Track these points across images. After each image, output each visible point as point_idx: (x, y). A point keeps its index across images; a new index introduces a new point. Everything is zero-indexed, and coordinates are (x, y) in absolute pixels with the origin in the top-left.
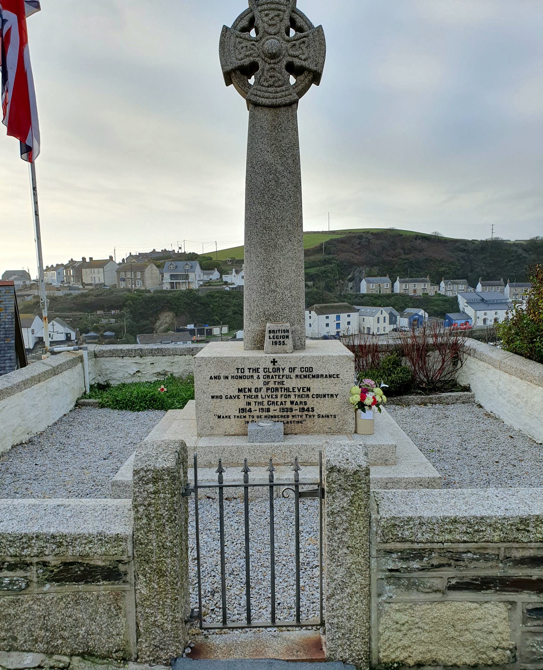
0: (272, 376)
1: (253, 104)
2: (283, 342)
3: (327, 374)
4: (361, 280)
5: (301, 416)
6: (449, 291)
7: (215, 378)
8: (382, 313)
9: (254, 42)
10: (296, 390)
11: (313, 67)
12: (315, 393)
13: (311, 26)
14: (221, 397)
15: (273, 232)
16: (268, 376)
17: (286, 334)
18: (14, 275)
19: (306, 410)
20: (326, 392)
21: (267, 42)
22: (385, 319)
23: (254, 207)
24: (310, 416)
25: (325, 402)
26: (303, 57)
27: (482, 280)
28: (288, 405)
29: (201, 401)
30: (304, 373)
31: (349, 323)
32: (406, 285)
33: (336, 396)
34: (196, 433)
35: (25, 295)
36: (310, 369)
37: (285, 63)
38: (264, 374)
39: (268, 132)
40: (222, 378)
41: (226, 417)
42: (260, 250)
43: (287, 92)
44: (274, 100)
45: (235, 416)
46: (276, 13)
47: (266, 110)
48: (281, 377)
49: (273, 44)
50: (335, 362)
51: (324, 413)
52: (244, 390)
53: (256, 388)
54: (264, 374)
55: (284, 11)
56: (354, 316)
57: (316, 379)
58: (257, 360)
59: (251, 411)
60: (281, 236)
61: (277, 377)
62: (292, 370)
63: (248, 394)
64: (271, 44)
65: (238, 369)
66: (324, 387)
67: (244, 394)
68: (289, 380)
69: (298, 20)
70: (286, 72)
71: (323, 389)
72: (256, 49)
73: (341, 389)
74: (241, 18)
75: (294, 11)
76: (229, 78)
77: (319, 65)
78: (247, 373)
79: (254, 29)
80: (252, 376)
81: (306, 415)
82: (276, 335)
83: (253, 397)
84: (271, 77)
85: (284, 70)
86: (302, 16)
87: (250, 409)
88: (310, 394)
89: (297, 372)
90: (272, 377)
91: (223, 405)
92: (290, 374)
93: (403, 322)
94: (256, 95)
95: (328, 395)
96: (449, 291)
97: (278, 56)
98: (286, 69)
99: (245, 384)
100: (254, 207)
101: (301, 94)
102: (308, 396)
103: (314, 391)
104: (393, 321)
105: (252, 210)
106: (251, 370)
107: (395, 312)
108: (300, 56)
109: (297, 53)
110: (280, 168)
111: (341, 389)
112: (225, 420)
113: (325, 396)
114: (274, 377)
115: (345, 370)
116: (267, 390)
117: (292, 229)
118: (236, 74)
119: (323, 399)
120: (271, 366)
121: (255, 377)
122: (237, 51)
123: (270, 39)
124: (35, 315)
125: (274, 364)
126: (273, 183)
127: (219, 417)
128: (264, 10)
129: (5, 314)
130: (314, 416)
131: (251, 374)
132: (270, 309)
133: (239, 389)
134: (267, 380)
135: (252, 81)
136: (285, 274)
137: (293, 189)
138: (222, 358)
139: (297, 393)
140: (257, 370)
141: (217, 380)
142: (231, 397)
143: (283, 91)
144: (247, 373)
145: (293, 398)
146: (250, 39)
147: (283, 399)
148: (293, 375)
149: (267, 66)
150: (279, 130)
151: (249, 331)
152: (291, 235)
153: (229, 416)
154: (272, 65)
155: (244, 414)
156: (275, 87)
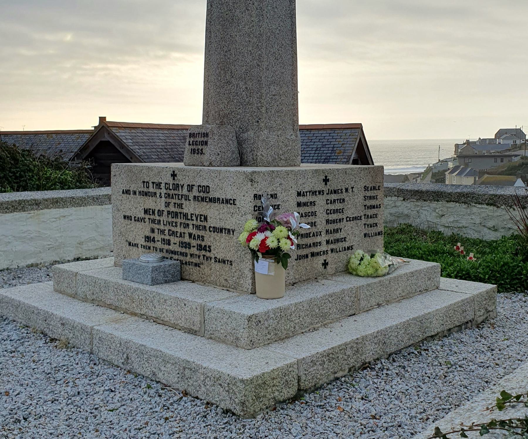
2: (202, 149)
5: (199, 257)
12: (212, 225)
17: (205, 139)
18: (506, 133)
28: (187, 239)
33: (233, 232)
35: (513, 156)
38: (165, 191)
51: (220, 256)
57: (213, 205)
59: (154, 241)
62: (190, 188)
81: (204, 256)
103: (211, 223)
111: (238, 222)
115: (242, 194)
116: (168, 214)
120: (170, 180)
124: (517, 178)
129: (341, 157)
132: (225, 107)
140: (158, 185)
145: (191, 230)
147: (183, 230)
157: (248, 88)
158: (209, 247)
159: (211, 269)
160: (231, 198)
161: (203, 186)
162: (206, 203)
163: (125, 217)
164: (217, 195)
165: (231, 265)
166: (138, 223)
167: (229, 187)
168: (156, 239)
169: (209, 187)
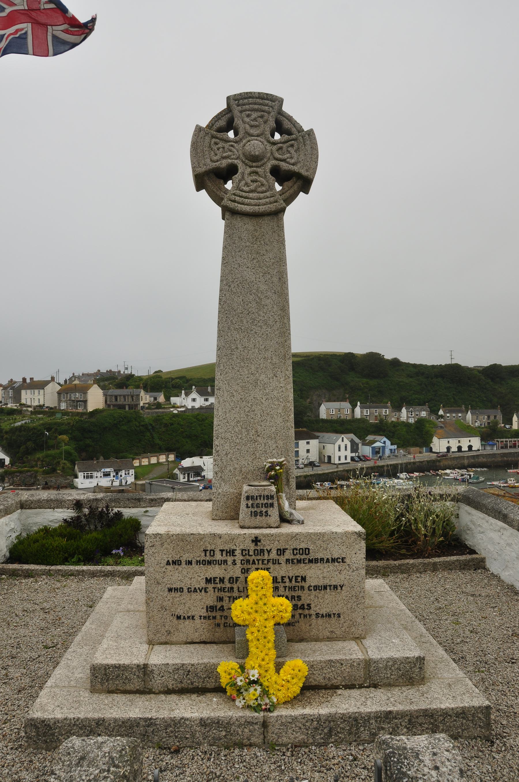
0: (254, 560)
1: (229, 213)
3: (329, 557)
4: (320, 405)
6: (410, 417)
7: (174, 563)
8: (343, 441)
9: (232, 143)
10: (287, 580)
11: (303, 172)
12: (313, 584)
13: (300, 130)
14: (181, 590)
15: (253, 365)
16: (248, 561)
17: (270, 501)
19: (300, 608)
20: (327, 582)
21: (249, 143)
22: (346, 447)
23: (229, 334)
24: (305, 616)
25: (326, 596)
26: (293, 161)
27: (444, 407)
29: (153, 596)
30: (298, 557)
31: (308, 451)
32: (367, 411)
34: (145, 639)
36: (306, 551)
37: (270, 166)
38: (241, 558)
39: (248, 244)
40: (183, 563)
41: (189, 617)
42: (236, 388)
43: (272, 199)
44: (257, 207)
45: (201, 616)
46: (259, 114)
47: (246, 220)
48: (266, 562)
49: (255, 145)
50: (340, 540)
51: (324, 611)
52: (214, 580)
53: (230, 578)
54: (241, 558)
55: (269, 113)
56: (314, 443)
57: (313, 565)
58: (233, 538)
60: (263, 370)
61: (260, 562)
62: (281, 552)
63: (219, 586)
64: (256, 146)
65: (205, 551)
66: (325, 575)
67: (213, 585)
68: (277, 566)
69: (285, 122)
70: (271, 176)
71: (324, 577)
72: (234, 150)
73: (348, 577)
74: (218, 118)
75: (280, 112)
76: (201, 181)
77: (311, 171)
78: (218, 556)
79: (233, 131)
80: (225, 562)
81: (300, 614)
82: (257, 502)
83: (227, 589)
84: (253, 181)
85: (269, 174)
86: (290, 119)
87: (222, 606)
88: (306, 585)
89: (288, 555)
90: (254, 562)
91: (184, 601)
92: (278, 557)
93: (366, 451)
94: (234, 201)
95: (330, 586)
96: (410, 417)
97: (262, 159)
98: (271, 173)
99: (216, 571)
100: (229, 334)
101: (289, 200)
102: (302, 588)
103: (311, 581)
104: (354, 448)
105: (227, 337)
106: (224, 553)
107: (357, 440)
108: (288, 160)
109: (285, 157)
110: (263, 287)
111: (348, 577)
112: (187, 622)
113: (325, 588)
114: (257, 562)
115: (354, 552)
117: (278, 361)
118: (209, 179)
119: (323, 592)
120: (252, 547)
121: (229, 563)
122: (212, 152)
123: (252, 140)
125: (256, 545)
126: (254, 305)
127: (179, 618)
128: (245, 111)
130: (310, 615)
131: (224, 558)
132: (248, 464)
133: (206, 578)
134: (245, 566)
135: (229, 185)
136: (269, 418)
137: (280, 312)
138: (183, 535)
139: (287, 584)
140: (231, 553)
141: (177, 566)
142: (195, 590)
143: (268, 197)
144: (218, 556)
146: (227, 141)
148: (282, 559)
149: (249, 170)
150: (262, 242)
151: (219, 494)
152: (276, 370)
153: (193, 617)
154: (255, 169)
155: (214, 614)
156: (258, 193)
157: (279, 447)
158: (309, 605)
159: (310, 625)
160: (339, 556)
161: (300, 549)
162: (304, 565)
163: (170, 590)
164: (319, 556)
165: (340, 617)
166: (194, 595)
167: (336, 546)
168: (225, 608)
169: (309, 549)
